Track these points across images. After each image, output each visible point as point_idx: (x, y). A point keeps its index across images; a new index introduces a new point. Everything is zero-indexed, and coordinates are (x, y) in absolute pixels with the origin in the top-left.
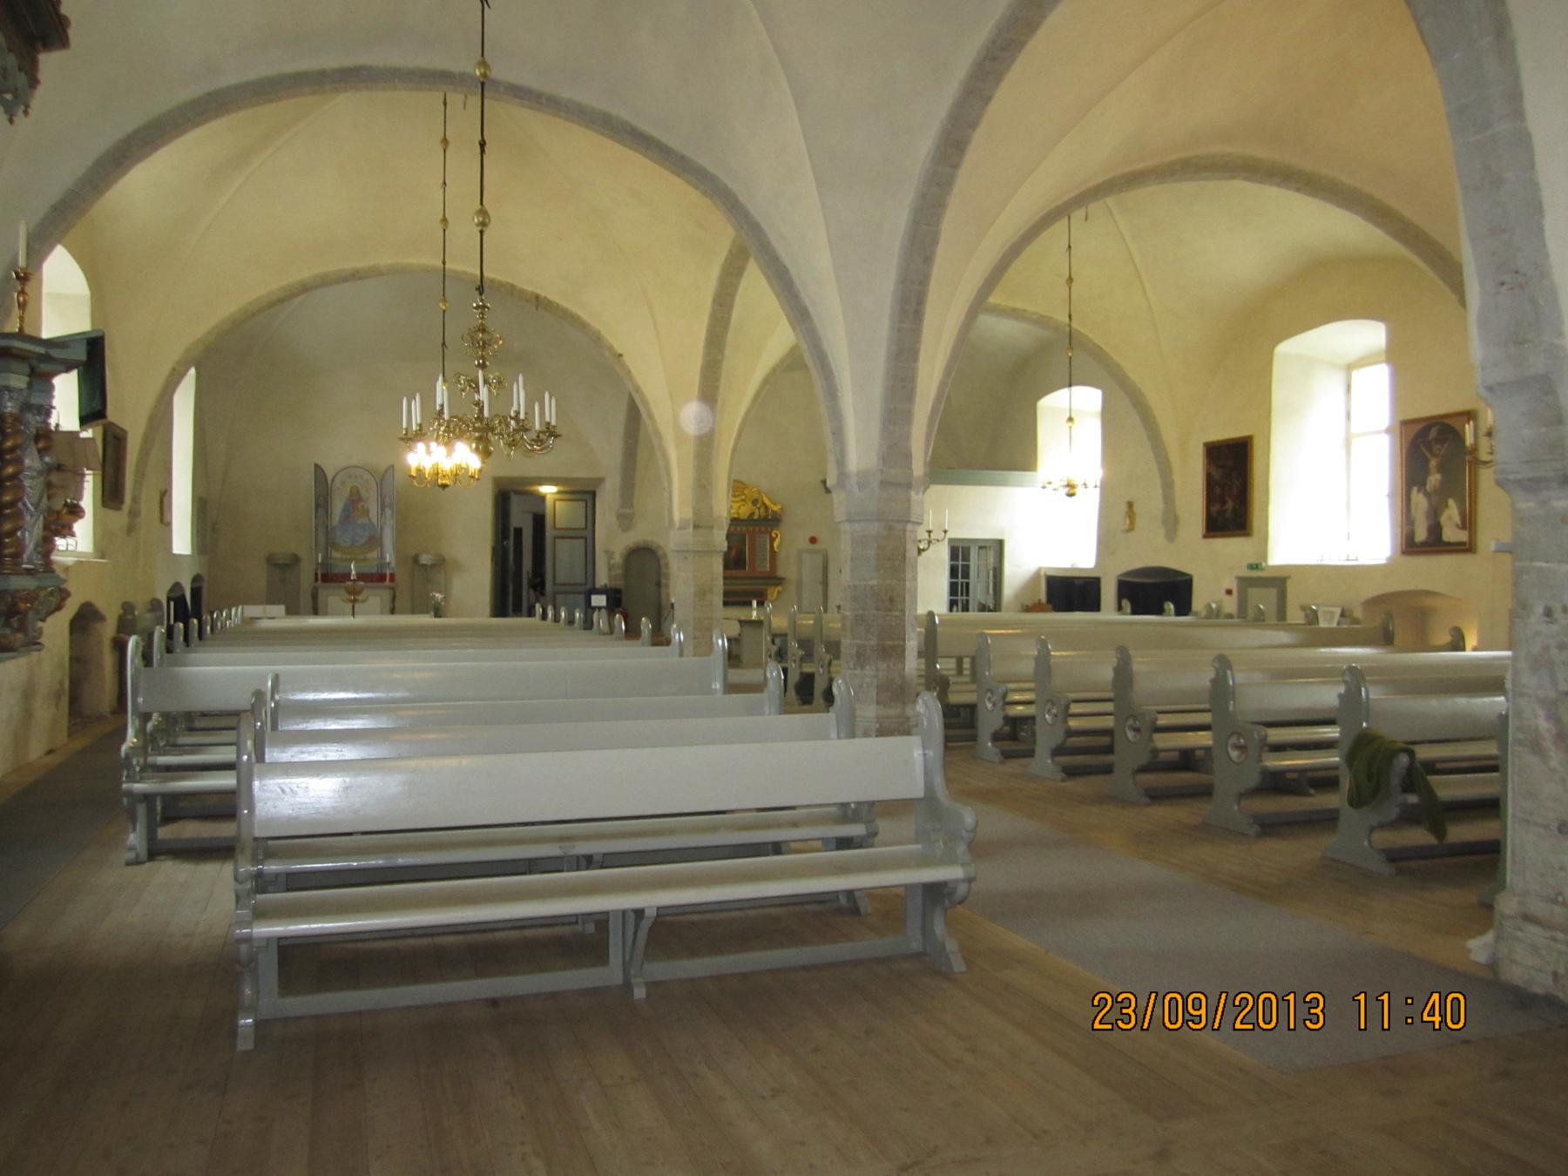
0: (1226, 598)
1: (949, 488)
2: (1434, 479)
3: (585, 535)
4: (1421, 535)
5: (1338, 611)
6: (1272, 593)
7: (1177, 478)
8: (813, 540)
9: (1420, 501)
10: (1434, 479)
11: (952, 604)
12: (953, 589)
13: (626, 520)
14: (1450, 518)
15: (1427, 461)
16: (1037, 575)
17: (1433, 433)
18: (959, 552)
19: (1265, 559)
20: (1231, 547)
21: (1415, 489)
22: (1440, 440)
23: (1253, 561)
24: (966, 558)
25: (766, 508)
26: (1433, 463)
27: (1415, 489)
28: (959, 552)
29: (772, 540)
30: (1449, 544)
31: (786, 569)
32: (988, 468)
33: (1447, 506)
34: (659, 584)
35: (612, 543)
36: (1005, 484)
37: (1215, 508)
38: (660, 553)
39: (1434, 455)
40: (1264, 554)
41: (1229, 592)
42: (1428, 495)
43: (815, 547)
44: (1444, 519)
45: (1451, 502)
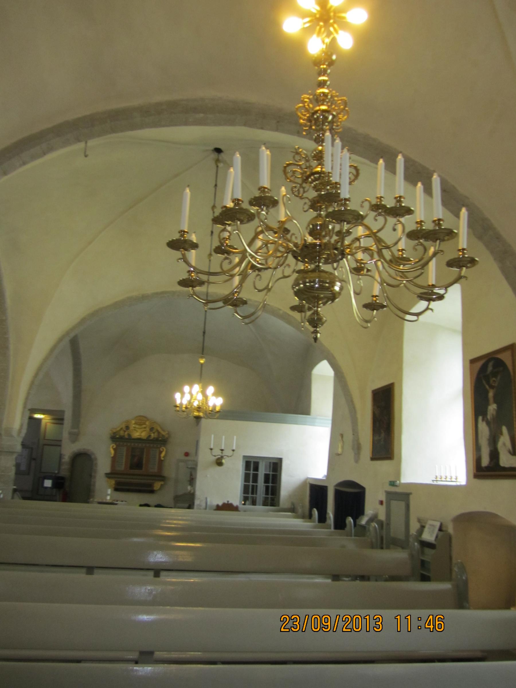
0: (379, 507)
1: (290, 425)
2: (492, 408)
3: (57, 443)
4: (485, 461)
5: (438, 524)
6: (402, 504)
7: (359, 416)
8: (187, 454)
9: (484, 428)
10: (492, 408)
11: (245, 499)
12: (246, 489)
13: (75, 437)
14: (504, 444)
15: (487, 392)
16: (305, 482)
17: (490, 368)
18: (251, 465)
19: (399, 480)
20: (384, 465)
21: (480, 418)
22: (494, 374)
23: (392, 479)
24: (256, 468)
25: (159, 433)
26: (491, 394)
27: (480, 418)
28: (251, 465)
29: (161, 452)
30: (504, 469)
31: (170, 471)
32: (273, 412)
33: (501, 433)
34: (91, 476)
35: (69, 450)
36: (296, 423)
37: (376, 438)
38: (93, 457)
39: (492, 387)
40: (398, 473)
41: (381, 503)
42: (488, 423)
43: (186, 458)
44: (500, 445)
45: (504, 429)
